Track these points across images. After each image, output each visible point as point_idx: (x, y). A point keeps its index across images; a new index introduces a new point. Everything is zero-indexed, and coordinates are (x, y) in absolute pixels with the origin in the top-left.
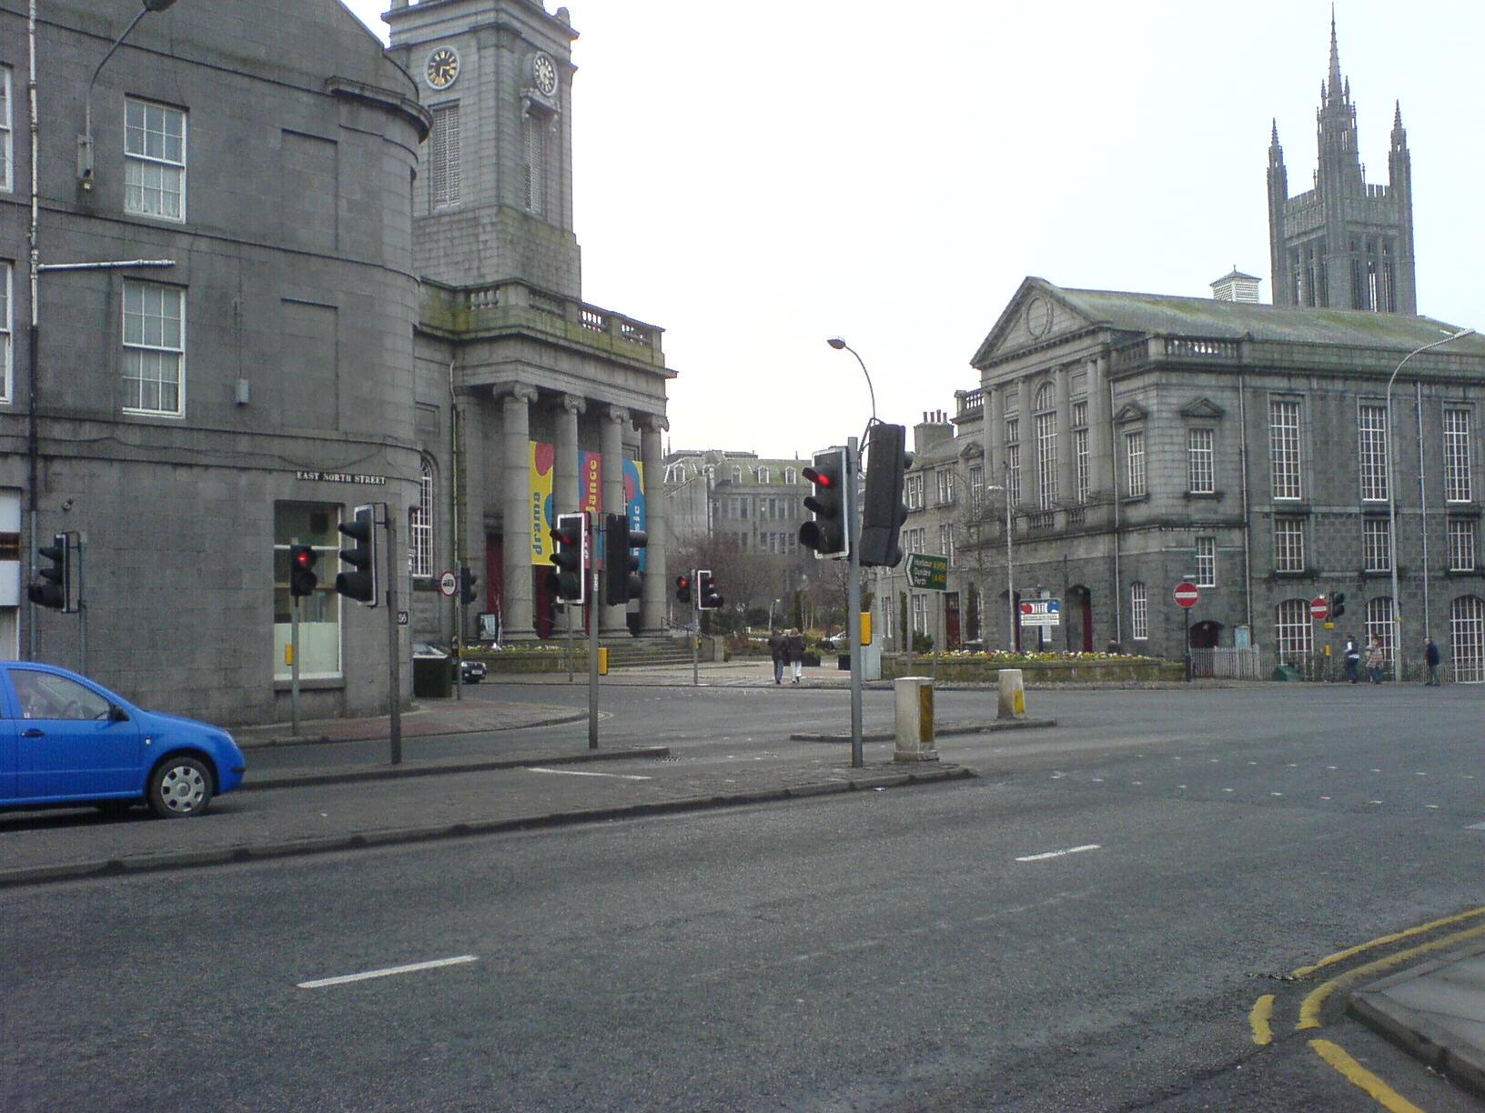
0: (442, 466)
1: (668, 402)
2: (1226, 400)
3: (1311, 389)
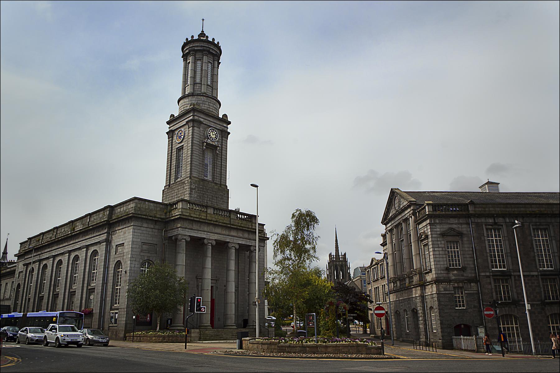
2: (464, 229)
3: (505, 222)
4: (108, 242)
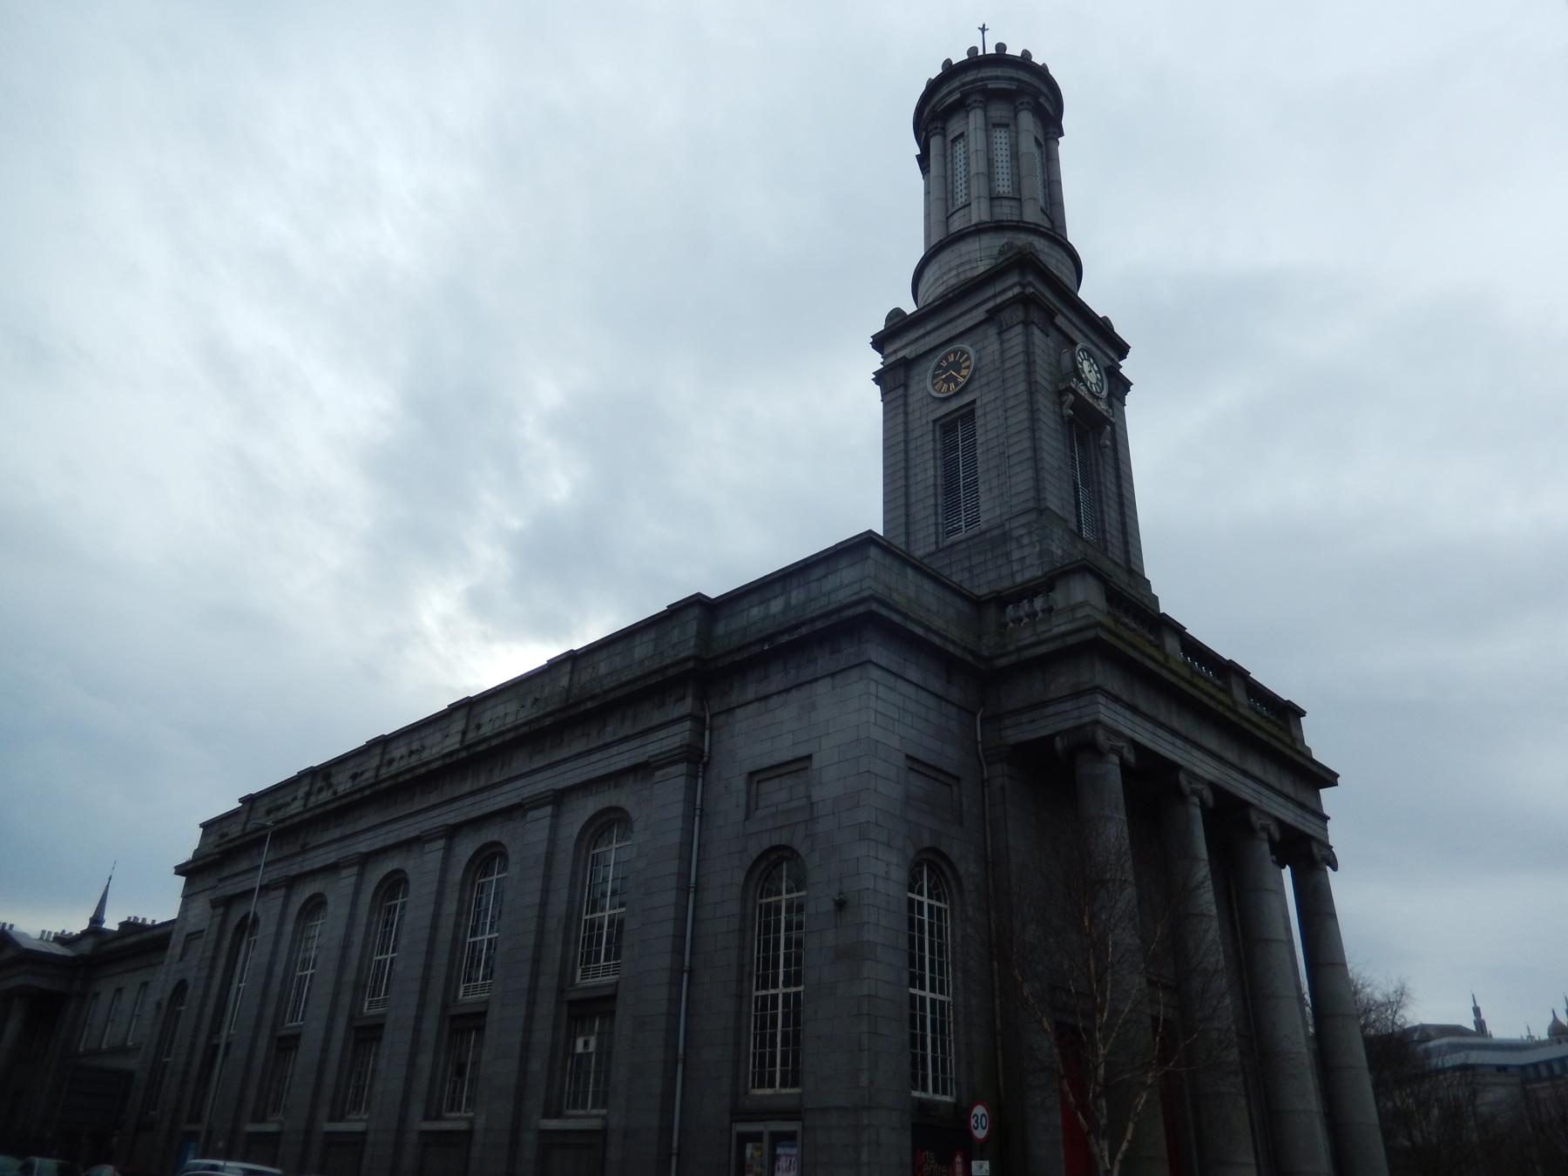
1: (1330, 824)
4: (696, 759)
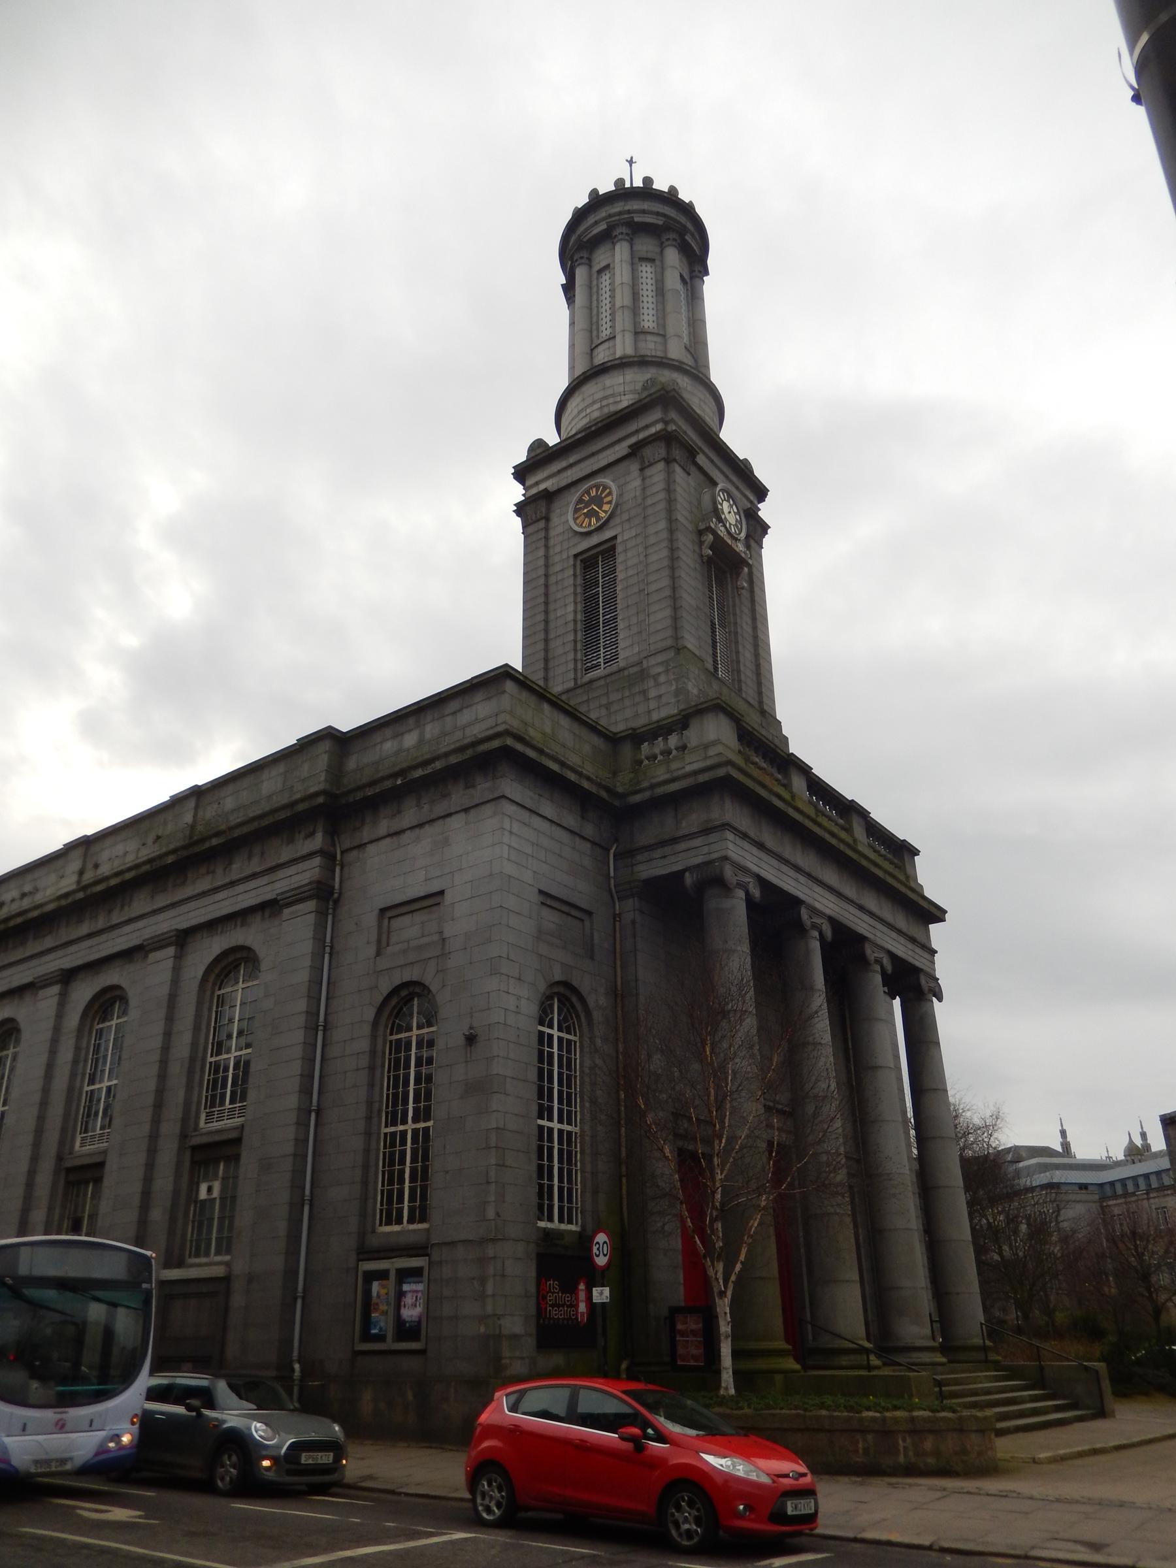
0: (597, 1016)
